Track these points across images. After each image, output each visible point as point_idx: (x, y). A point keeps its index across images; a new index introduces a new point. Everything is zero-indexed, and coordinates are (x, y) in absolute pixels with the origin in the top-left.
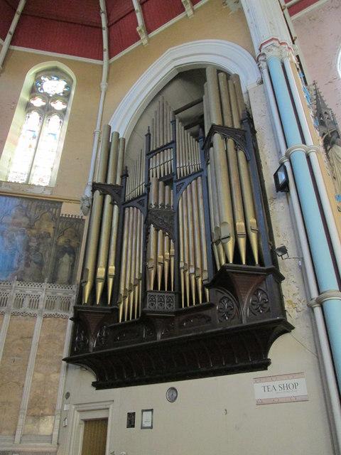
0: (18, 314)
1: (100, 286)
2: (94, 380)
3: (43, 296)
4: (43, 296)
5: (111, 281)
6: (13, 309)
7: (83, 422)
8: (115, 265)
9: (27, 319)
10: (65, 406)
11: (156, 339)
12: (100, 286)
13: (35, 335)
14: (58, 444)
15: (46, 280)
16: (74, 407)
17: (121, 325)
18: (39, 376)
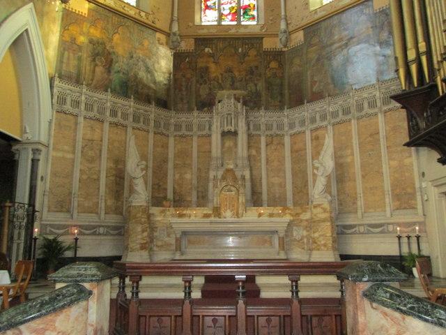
0: (362, 117)
1: (414, 68)
2: (439, 157)
3: (378, 95)
4: (378, 95)
5: (424, 59)
6: (357, 114)
7: (442, 195)
8: (425, 41)
9: (371, 119)
10: (423, 184)
11: (439, 95)
12: (414, 68)
13: (381, 131)
14: (424, 215)
15: (263, 108)
16: (430, 183)
17: (442, 97)
18: (394, 163)
